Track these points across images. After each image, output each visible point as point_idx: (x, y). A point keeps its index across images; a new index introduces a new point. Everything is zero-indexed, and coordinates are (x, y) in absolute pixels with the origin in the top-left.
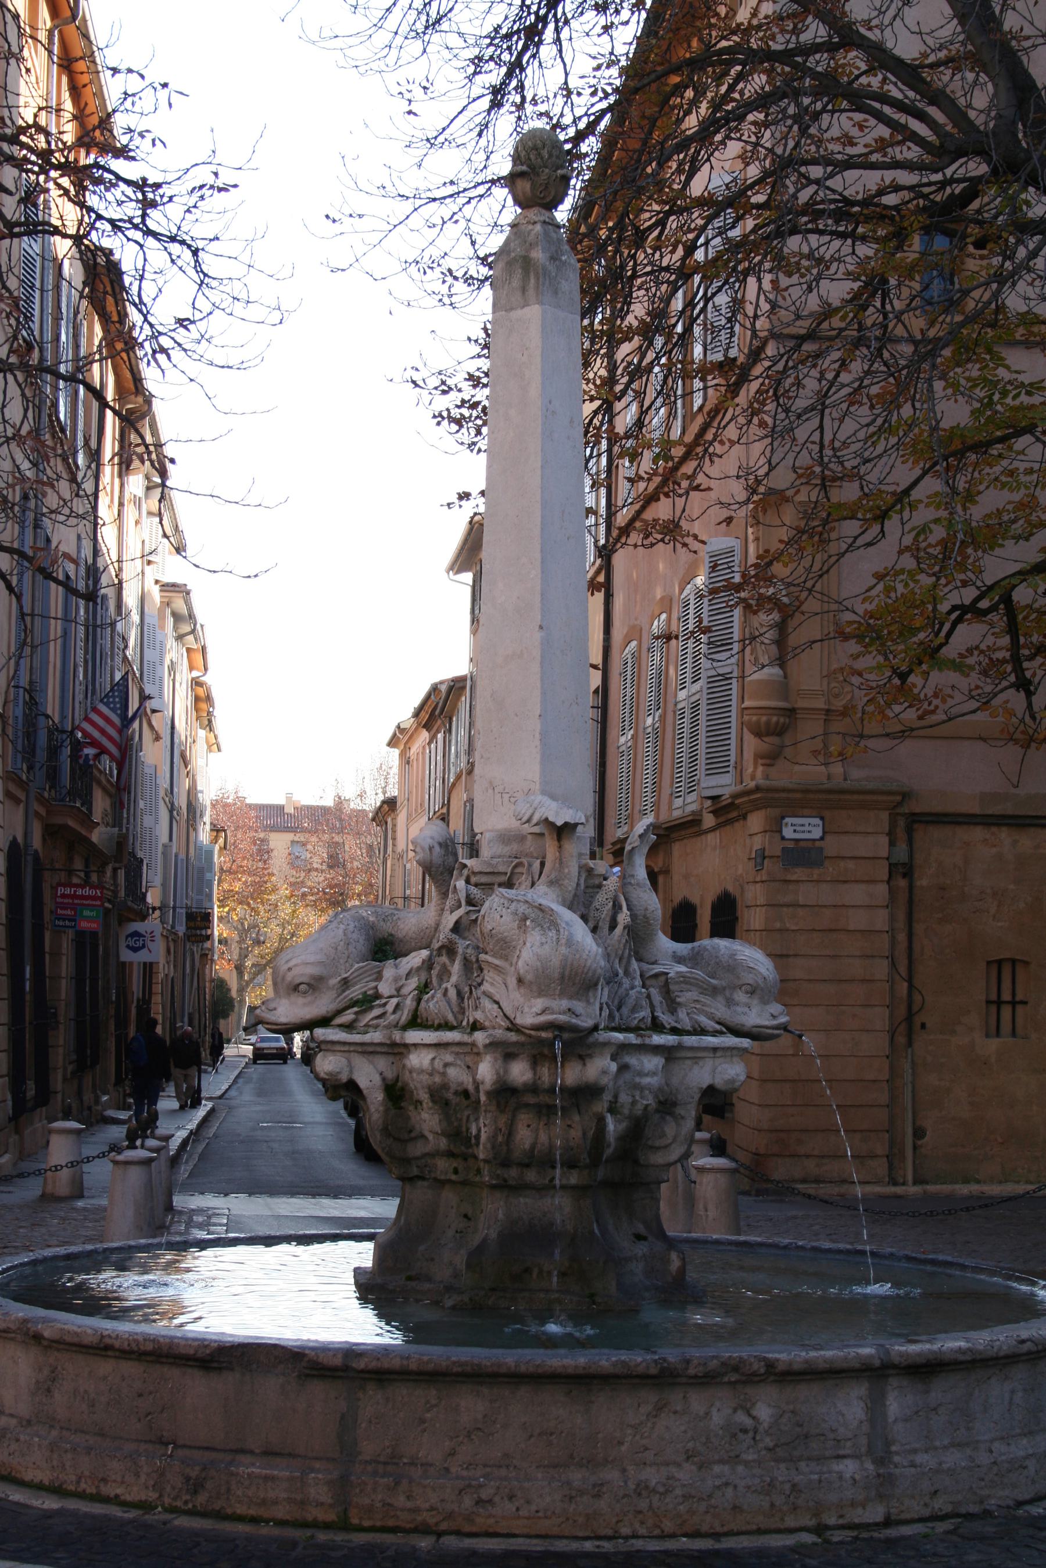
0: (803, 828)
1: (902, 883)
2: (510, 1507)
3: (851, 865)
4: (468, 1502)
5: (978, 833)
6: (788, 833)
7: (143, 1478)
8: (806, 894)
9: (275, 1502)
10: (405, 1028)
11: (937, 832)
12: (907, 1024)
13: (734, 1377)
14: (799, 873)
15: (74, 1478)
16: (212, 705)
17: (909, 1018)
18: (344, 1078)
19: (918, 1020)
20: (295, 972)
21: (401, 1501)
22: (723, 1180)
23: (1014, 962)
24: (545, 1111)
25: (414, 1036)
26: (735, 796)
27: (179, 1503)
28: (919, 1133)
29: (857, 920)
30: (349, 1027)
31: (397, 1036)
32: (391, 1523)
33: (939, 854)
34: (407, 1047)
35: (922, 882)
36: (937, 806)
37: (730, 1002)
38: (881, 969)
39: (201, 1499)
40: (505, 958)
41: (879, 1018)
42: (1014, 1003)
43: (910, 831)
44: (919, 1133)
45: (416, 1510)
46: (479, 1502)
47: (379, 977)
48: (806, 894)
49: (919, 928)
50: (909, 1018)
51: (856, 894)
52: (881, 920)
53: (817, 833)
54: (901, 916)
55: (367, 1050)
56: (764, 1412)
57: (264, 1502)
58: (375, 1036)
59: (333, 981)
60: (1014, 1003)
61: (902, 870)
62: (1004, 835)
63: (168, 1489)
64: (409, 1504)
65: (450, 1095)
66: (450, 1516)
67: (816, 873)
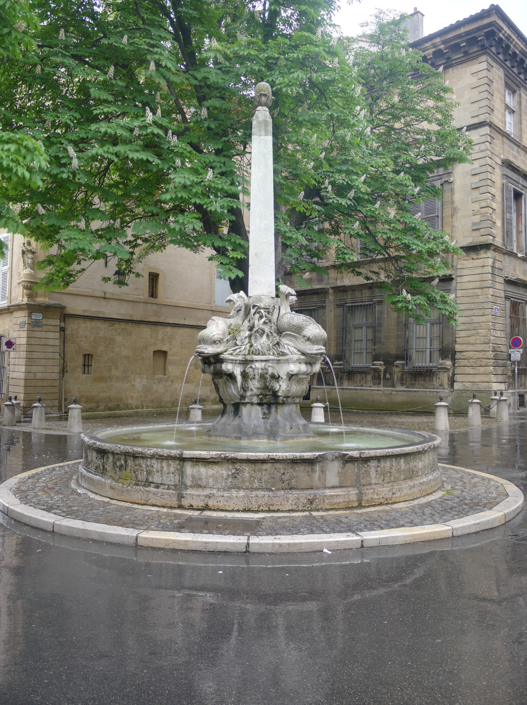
0: (38, 316)
1: (62, 333)
3: (50, 327)
5: (81, 321)
6: (33, 317)
7: (290, 502)
8: (37, 334)
12: (63, 371)
15: (257, 506)
17: (63, 370)
19: (65, 370)
20: (215, 336)
21: (375, 497)
22: (80, 410)
23: (88, 355)
25: (256, 357)
27: (305, 508)
29: (51, 342)
30: (231, 354)
31: (249, 358)
32: (373, 504)
33: (72, 326)
34: (252, 361)
35: (68, 332)
38: (57, 356)
40: (298, 333)
41: (57, 369)
42: (88, 365)
48: (37, 334)
49: (66, 345)
50: (63, 370)
51: (51, 335)
52: (57, 342)
53: (41, 318)
54: (62, 342)
58: (240, 358)
59: (225, 340)
60: (88, 365)
61: (63, 330)
63: (301, 504)
64: (377, 497)
65: (268, 376)
67: (40, 329)
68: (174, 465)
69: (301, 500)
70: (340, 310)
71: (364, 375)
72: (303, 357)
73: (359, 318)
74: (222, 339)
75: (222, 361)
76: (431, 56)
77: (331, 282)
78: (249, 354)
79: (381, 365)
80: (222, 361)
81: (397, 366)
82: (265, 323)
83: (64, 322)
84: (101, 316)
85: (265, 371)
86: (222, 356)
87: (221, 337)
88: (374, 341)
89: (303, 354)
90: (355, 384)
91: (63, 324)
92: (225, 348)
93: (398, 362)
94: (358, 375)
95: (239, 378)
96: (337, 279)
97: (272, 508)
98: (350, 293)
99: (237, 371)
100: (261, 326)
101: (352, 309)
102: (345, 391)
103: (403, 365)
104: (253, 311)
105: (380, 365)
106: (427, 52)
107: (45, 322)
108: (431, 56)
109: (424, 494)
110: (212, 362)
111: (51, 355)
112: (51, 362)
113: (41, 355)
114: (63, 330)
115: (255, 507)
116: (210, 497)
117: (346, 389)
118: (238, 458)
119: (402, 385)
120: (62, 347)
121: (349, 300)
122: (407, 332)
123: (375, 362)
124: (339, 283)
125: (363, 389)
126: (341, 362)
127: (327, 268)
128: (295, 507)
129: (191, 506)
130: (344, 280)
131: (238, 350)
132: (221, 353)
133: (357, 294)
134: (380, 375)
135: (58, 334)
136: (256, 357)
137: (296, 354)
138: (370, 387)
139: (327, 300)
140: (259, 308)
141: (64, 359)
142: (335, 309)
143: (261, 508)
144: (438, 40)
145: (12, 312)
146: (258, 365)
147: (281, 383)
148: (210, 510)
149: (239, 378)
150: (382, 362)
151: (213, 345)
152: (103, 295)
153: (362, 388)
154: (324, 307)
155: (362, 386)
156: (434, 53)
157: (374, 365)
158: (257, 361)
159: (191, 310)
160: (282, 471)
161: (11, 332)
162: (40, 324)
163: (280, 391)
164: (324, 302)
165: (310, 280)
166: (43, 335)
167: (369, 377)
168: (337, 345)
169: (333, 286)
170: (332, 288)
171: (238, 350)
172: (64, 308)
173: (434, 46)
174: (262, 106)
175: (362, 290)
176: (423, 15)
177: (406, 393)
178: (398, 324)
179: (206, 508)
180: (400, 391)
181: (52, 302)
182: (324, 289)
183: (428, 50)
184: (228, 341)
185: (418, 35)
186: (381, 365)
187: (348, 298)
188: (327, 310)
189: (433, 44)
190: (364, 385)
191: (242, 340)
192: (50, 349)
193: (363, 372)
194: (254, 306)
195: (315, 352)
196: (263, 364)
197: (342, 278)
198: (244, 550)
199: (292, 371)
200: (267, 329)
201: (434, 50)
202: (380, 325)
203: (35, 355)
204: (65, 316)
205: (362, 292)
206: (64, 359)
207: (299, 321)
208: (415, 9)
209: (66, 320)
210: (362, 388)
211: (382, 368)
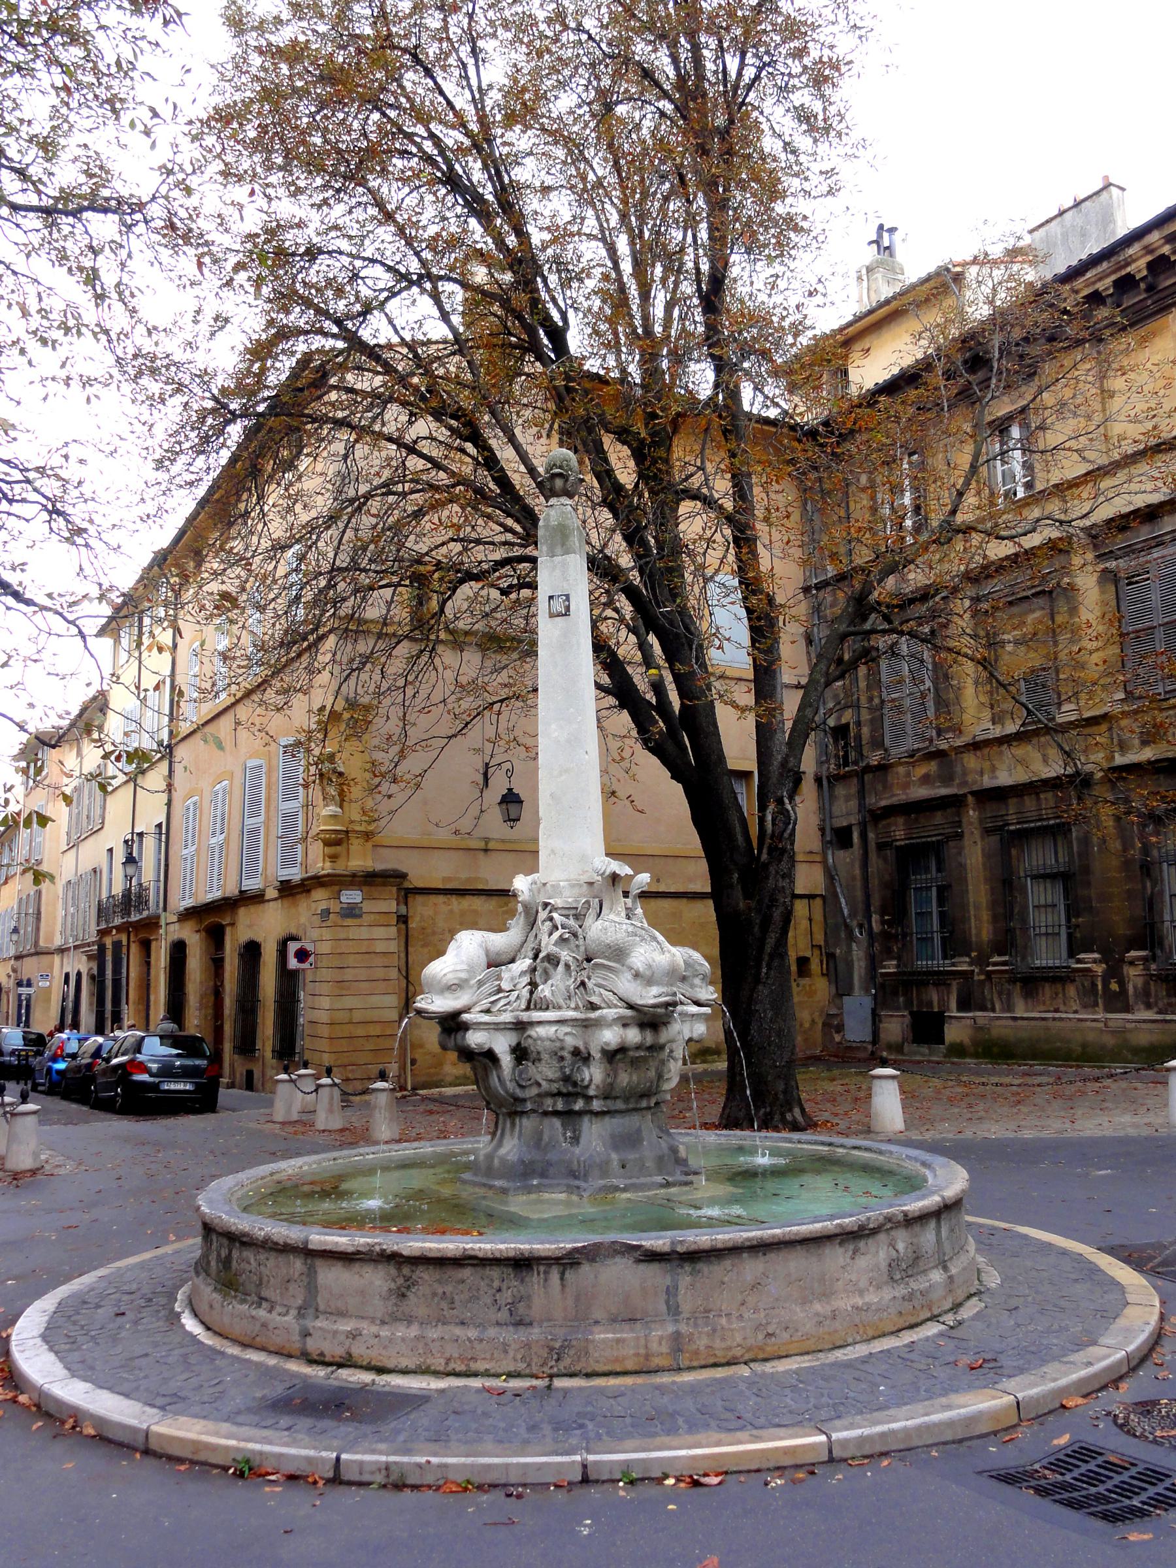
2: (786, 1336)
4: (760, 1336)
5: (441, 899)
6: (343, 899)
7: (511, 1353)
8: (354, 933)
9: (624, 1358)
10: (528, 1008)
11: (420, 899)
13: (888, 1226)
14: (349, 922)
15: (443, 1361)
16: (603, 786)
18: (487, 1047)
20: (450, 976)
24: (635, 1063)
25: (537, 1015)
26: (303, 880)
28: (413, 1062)
29: (380, 947)
30: (488, 1011)
31: (525, 1016)
34: (531, 1024)
35: (412, 925)
36: (421, 885)
37: (692, 986)
38: (394, 974)
39: (566, 1362)
40: (618, 961)
43: (406, 898)
44: (413, 1062)
45: (729, 1348)
46: (769, 1335)
47: (499, 978)
48: (354, 933)
51: (380, 932)
52: (393, 947)
53: (359, 900)
55: (497, 1027)
56: (901, 1246)
57: (616, 1360)
58: (507, 1017)
59: (473, 982)
61: (403, 919)
62: (454, 900)
64: (723, 1345)
65: (565, 1054)
66: (749, 1350)
67: (357, 921)
68: (298, 1265)
69: (534, 1349)
70: (994, 839)
71: (1059, 986)
72: (629, 1013)
73: (1040, 856)
74: (466, 981)
75: (465, 1027)
76: (1145, 273)
77: (970, 779)
78: (528, 1008)
79: (1095, 961)
80: (465, 1027)
81: (1132, 963)
82: (562, 940)
83: (406, 904)
84: (480, 887)
85: (558, 1044)
86: (466, 1017)
87: (463, 975)
88: (1072, 911)
89: (630, 1006)
90: (1042, 1008)
91: (403, 910)
92: (475, 999)
93: (1133, 953)
94: (1047, 986)
95: (506, 1060)
96: (982, 773)
97: (474, 1366)
98: (1012, 802)
99: (502, 1045)
100: (555, 949)
101: (1024, 836)
102: (1020, 1022)
103: (1145, 959)
104: (543, 915)
105: (1090, 960)
106: (1133, 266)
107: (367, 907)
108: (1145, 273)
109: (871, 1333)
110: (452, 1024)
111: (380, 973)
112: (381, 986)
113: (363, 974)
114: (403, 919)
115: (438, 1363)
116: (354, 1337)
117: (1023, 1018)
118: (405, 1253)
119: (1149, 1006)
120: (403, 955)
121: (1012, 818)
122: (1149, 885)
123: (1081, 956)
124: (987, 782)
125: (1061, 1019)
126: (1006, 958)
127: (959, 750)
128: (521, 1366)
129: (322, 1354)
130: (998, 773)
131: (502, 1002)
132: (467, 1010)
133: (1029, 803)
134: (1094, 985)
135: (394, 929)
136: (537, 1015)
137: (616, 1006)
138: (1076, 1012)
139: (964, 820)
140: (555, 909)
141: (407, 978)
142: (982, 838)
143: (452, 1366)
144: (1155, 237)
145: (309, 891)
146: (541, 1031)
147: (592, 1069)
148: (356, 1366)
149: (506, 1060)
150: (1096, 956)
151: (447, 994)
152: (482, 845)
153: (1057, 1015)
154: (959, 836)
155: (1057, 1011)
156: (1150, 266)
157: (1079, 961)
158: (540, 1023)
159: (670, 860)
160: (496, 1284)
161: (309, 929)
162: (357, 912)
163: (593, 1087)
164: (959, 824)
165: (926, 779)
166: (364, 933)
167: (1072, 991)
168: (995, 919)
169: (975, 788)
170: (973, 793)
171: (502, 1002)
172: (403, 876)
173: (1148, 250)
174: (558, 496)
175: (1037, 794)
176: (1123, 189)
177: (1160, 1026)
178: (1127, 864)
179: (347, 1362)
180: (1144, 1021)
181: (380, 867)
182: (955, 795)
183: (1134, 261)
184: (480, 983)
185: (1113, 232)
186: (1095, 961)
187: (1012, 815)
188: (967, 841)
189: (1145, 248)
190: (1062, 1008)
191: (512, 979)
192: (379, 961)
193: (1058, 978)
194: (546, 905)
195: (652, 1001)
196: (553, 1029)
197: (993, 769)
198: (331, 1474)
199: (607, 1044)
200: (565, 955)
201: (1149, 258)
202: (1086, 870)
203: (349, 974)
204: (408, 893)
205: (1038, 799)
206: (407, 978)
207: (619, 936)
208: (1106, 178)
209: (410, 900)
210: (1057, 1015)
211: (1099, 969)
